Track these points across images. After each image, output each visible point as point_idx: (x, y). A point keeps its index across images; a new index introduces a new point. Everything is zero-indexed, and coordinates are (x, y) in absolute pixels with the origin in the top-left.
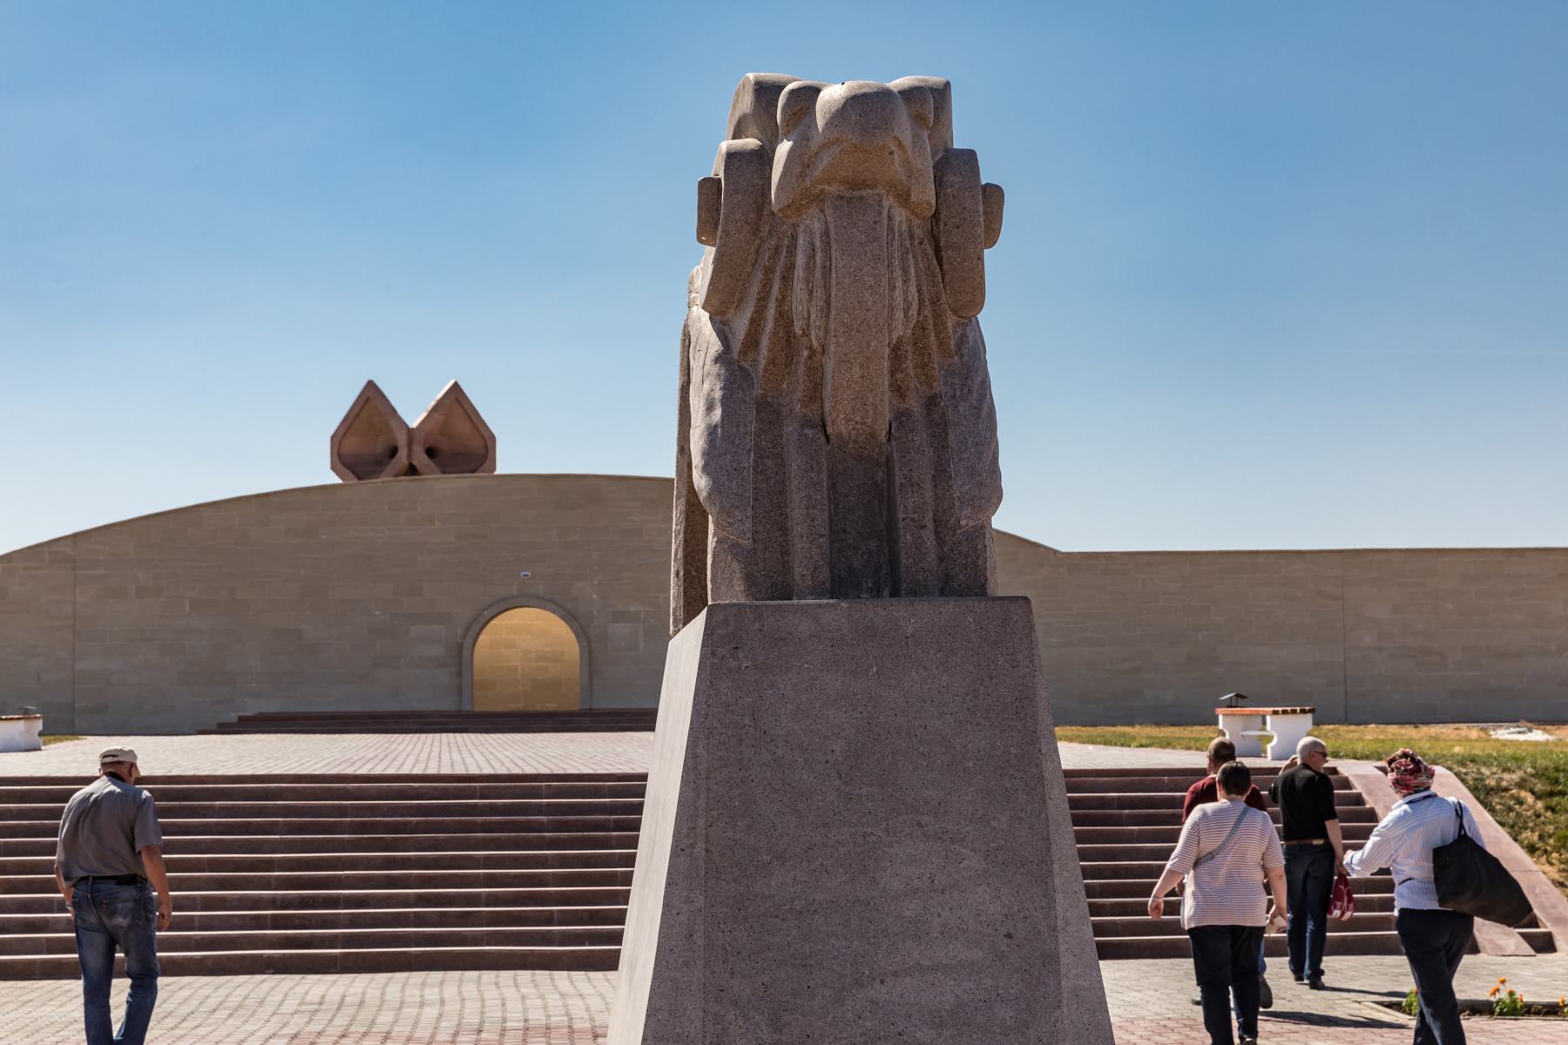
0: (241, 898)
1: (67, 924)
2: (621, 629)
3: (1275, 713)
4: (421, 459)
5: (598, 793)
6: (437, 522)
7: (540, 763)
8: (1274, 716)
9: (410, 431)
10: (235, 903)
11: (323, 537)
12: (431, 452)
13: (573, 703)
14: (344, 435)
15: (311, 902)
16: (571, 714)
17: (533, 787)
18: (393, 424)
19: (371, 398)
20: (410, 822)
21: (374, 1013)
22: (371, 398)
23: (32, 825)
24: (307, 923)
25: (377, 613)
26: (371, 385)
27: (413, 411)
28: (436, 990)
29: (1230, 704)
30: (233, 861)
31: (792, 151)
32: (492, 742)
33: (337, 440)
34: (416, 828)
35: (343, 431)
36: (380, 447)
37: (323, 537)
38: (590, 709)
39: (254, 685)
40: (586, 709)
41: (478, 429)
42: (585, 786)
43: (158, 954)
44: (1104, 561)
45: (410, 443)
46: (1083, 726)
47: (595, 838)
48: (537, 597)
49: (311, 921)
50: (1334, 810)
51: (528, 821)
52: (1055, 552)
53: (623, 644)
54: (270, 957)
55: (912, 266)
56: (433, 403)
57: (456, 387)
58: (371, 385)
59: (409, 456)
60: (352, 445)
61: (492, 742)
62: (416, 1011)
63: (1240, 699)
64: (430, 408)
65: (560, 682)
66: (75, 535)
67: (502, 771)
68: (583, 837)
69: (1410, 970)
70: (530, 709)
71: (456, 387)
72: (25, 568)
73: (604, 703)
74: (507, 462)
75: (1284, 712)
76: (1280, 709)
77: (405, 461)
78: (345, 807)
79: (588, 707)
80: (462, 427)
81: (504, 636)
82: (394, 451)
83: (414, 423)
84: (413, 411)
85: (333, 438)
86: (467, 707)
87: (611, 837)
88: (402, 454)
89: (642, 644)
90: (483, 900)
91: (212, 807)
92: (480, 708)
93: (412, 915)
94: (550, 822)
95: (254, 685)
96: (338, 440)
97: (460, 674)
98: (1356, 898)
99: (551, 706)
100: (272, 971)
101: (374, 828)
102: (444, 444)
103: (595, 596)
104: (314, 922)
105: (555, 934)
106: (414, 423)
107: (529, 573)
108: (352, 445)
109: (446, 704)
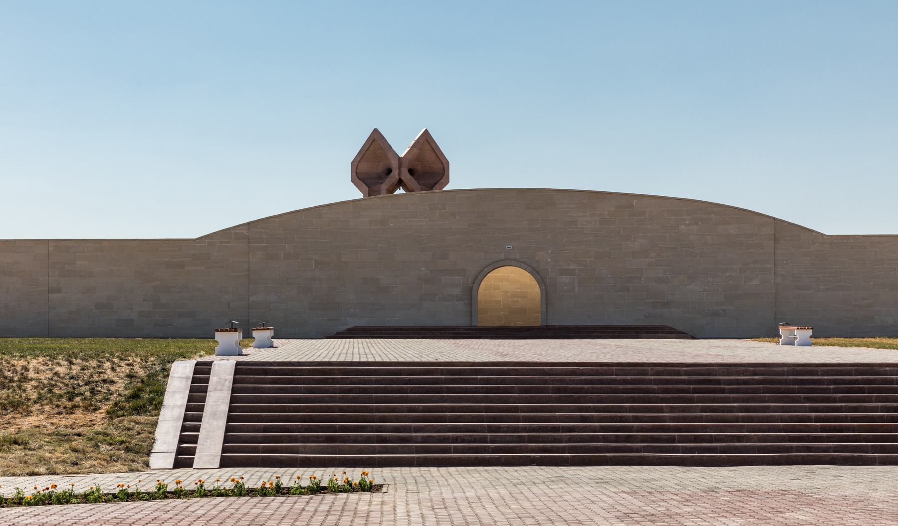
0: (508, 427)
1: (422, 439)
2: (565, 279)
3: (798, 329)
4: (406, 177)
5: (678, 373)
6: (457, 217)
7: (397, 353)
8: (798, 330)
9: (400, 159)
10: (505, 429)
11: (391, 225)
12: (411, 172)
13: (536, 321)
14: (359, 161)
15: (544, 429)
16: (539, 328)
17: (644, 370)
18: (390, 155)
20: (584, 388)
21: (316, 505)
23: (386, 387)
24: (546, 440)
25: (422, 269)
26: (376, 131)
27: (402, 147)
29: (783, 325)
30: (497, 407)
32: (383, 344)
33: (356, 164)
34: (587, 391)
35: (358, 159)
36: (381, 169)
37: (391, 225)
38: (547, 326)
39: (352, 310)
40: (544, 326)
41: (439, 158)
44: (852, 241)
45: (400, 166)
46: (845, 338)
47: (685, 397)
48: (515, 260)
49: (548, 439)
51: (647, 388)
52: (823, 235)
53: (565, 288)
54: (534, 457)
56: (413, 142)
59: (399, 174)
60: (364, 167)
61: (383, 344)
62: (354, 506)
63: (787, 324)
64: (411, 145)
65: (526, 309)
66: (249, 223)
67: (386, 360)
68: (679, 397)
70: (508, 325)
72: (221, 242)
73: (555, 321)
74: (457, 181)
75: (801, 328)
76: (800, 327)
77: (397, 177)
78: (547, 379)
79: (545, 324)
80: (429, 156)
81: (493, 283)
82: (389, 171)
83: (402, 155)
84: (402, 147)
85: (352, 163)
86: (474, 324)
87: (694, 397)
88: (395, 173)
89: (577, 288)
91: (476, 379)
92: (481, 324)
93: (601, 437)
94: (763, 388)
95: (352, 310)
97: (471, 304)
99: (520, 324)
100: (535, 464)
101: (565, 390)
102: (419, 167)
103: (549, 260)
104: (549, 439)
105: (679, 447)
106: (402, 155)
107: (511, 246)
108: (364, 167)
109: (463, 322)
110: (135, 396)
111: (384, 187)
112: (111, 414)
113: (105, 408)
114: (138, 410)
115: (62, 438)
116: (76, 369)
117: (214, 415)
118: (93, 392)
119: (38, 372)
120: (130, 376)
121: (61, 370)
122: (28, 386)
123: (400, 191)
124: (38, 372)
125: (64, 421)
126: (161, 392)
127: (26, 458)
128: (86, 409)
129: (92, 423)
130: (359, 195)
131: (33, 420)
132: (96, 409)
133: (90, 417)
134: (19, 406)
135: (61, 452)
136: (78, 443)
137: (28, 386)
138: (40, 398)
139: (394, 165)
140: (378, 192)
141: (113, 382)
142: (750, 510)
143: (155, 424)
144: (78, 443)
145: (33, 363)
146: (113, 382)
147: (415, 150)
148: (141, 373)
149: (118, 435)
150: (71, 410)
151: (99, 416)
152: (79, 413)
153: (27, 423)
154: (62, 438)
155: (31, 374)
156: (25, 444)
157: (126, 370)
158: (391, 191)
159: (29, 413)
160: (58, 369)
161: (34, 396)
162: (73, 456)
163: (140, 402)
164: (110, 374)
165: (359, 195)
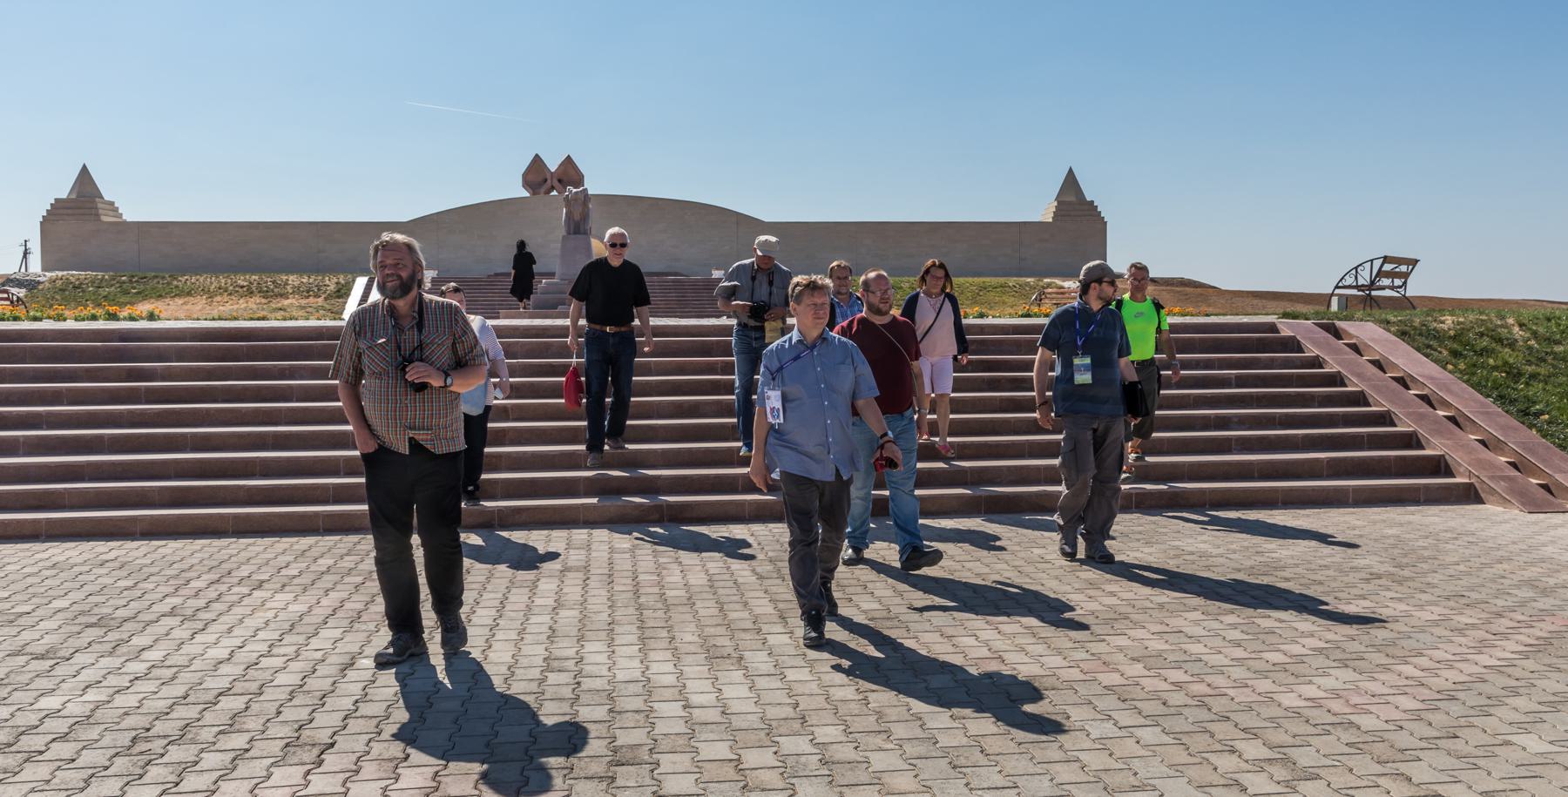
4: (556, 183)
12: (560, 181)
19: (537, 160)
22: (537, 160)
26: (537, 155)
27: (553, 164)
28: (556, 582)
30: (1257, 376)
31: (1472, 434)
36: (540, 179)
42: (187, 347)
43: (1157, 412)
50: (965, 339)
55: (1561, 464)
57: (569, 156)
58: (537, 155)
60: (530, 178)
69: (1119, 396)
71: (569, 156)
77: (550, 185)
82: (546, 180)
83: (553, 170)
84: (553, 164)
88: (549, 181)
90: (1233, 382)
96: (525, 176)
98: (640, 383)
106: (553, 170)
108: (530, 178)
110: (338, 291)
111: (543, 190)
112: (326, 299)
113: (323, 296)
114: (339, 297)
115: (302, 308)
116: (311, 280)
117: (424, 584)
118: (319, 290)
119: (293, 281)
120: (337, 283)
121: (304, 281)
122: (288, 287)
123: (554, 193)
124: (293, 281)
125: (303, 302)
126: (350, 290)
127: (317, 282)
128: (315, 296)
129: (317, 302)
130: (528, 195)
131: (289, 301)
132: (320, 296)
133: (316, 300)
134: (284, 296)
135: (301, 313)
136: (309, 310)
137: (288, 287)
138: (294, 292)
139: (549, 177)
140: (539, 194)
141: (328, 286)
142: (1445, 590)
143: (346, 303)
144: (309, 310)
145: (291, 278)
146: (328, 286)
147: (562, 167)
148: (343, 282)
149: (328, 307)
150: (308, 297)
151: (320, 300)
152: (311, 298)
153: (286, 302)
154: (302, 308)
155: (290, 282)
156: (285, 310)
157: (336, 280)
158: (548, 192)
159: (288, 298)
160: (303, 280)
161: (291, 291)
162: (306, 314)
163: (340, 294)
164: (327, 282)
165: (528, 195)
